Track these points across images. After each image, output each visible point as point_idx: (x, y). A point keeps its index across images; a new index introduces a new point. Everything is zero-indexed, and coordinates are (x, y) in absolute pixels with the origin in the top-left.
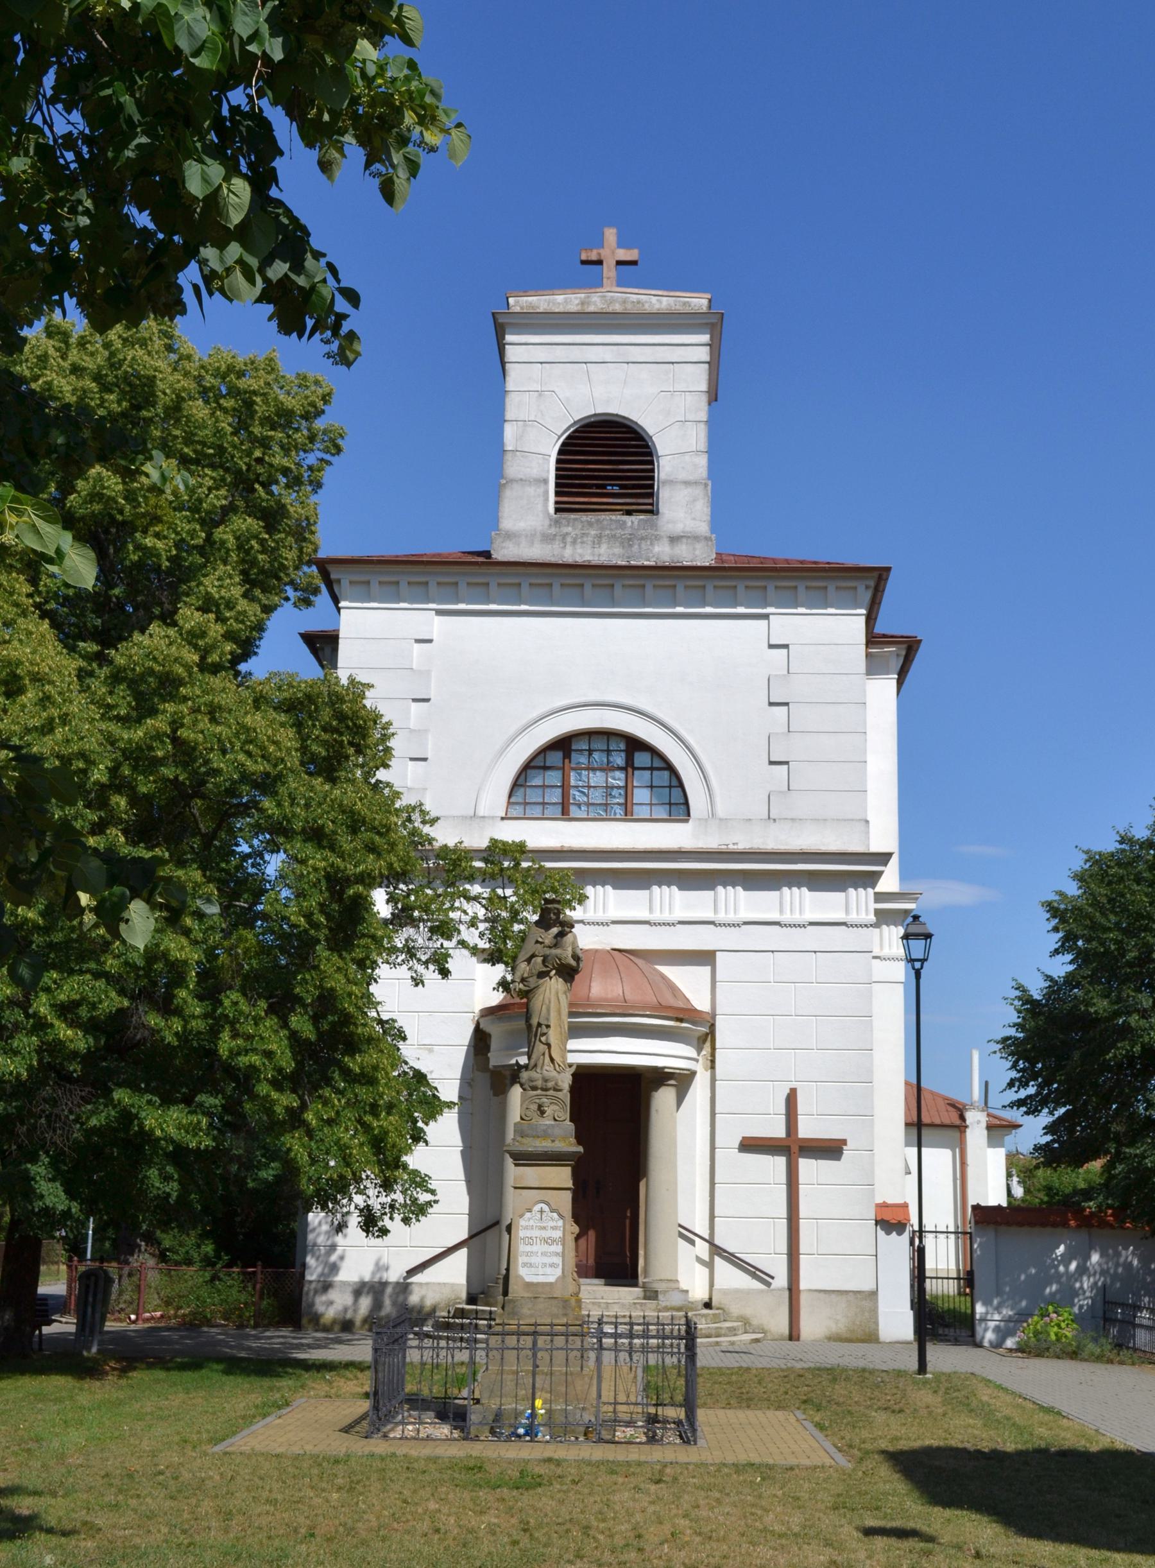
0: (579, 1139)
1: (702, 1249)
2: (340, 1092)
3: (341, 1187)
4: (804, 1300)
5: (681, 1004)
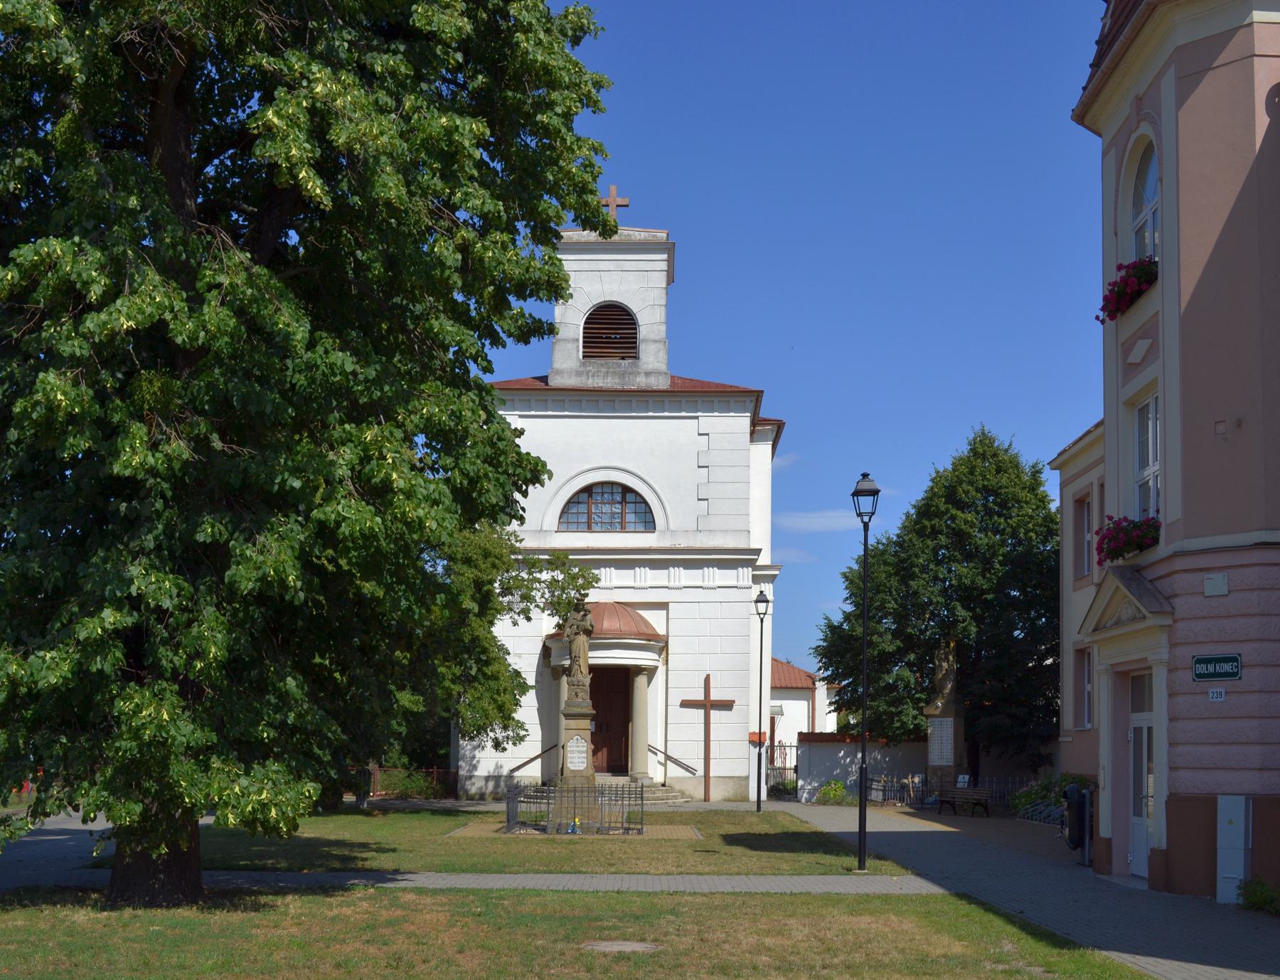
0: (594, 707)
1: (661, 757)
2: (483, 685)
3: (482, 729)
4: (712, 782)
5: (650, 632)
